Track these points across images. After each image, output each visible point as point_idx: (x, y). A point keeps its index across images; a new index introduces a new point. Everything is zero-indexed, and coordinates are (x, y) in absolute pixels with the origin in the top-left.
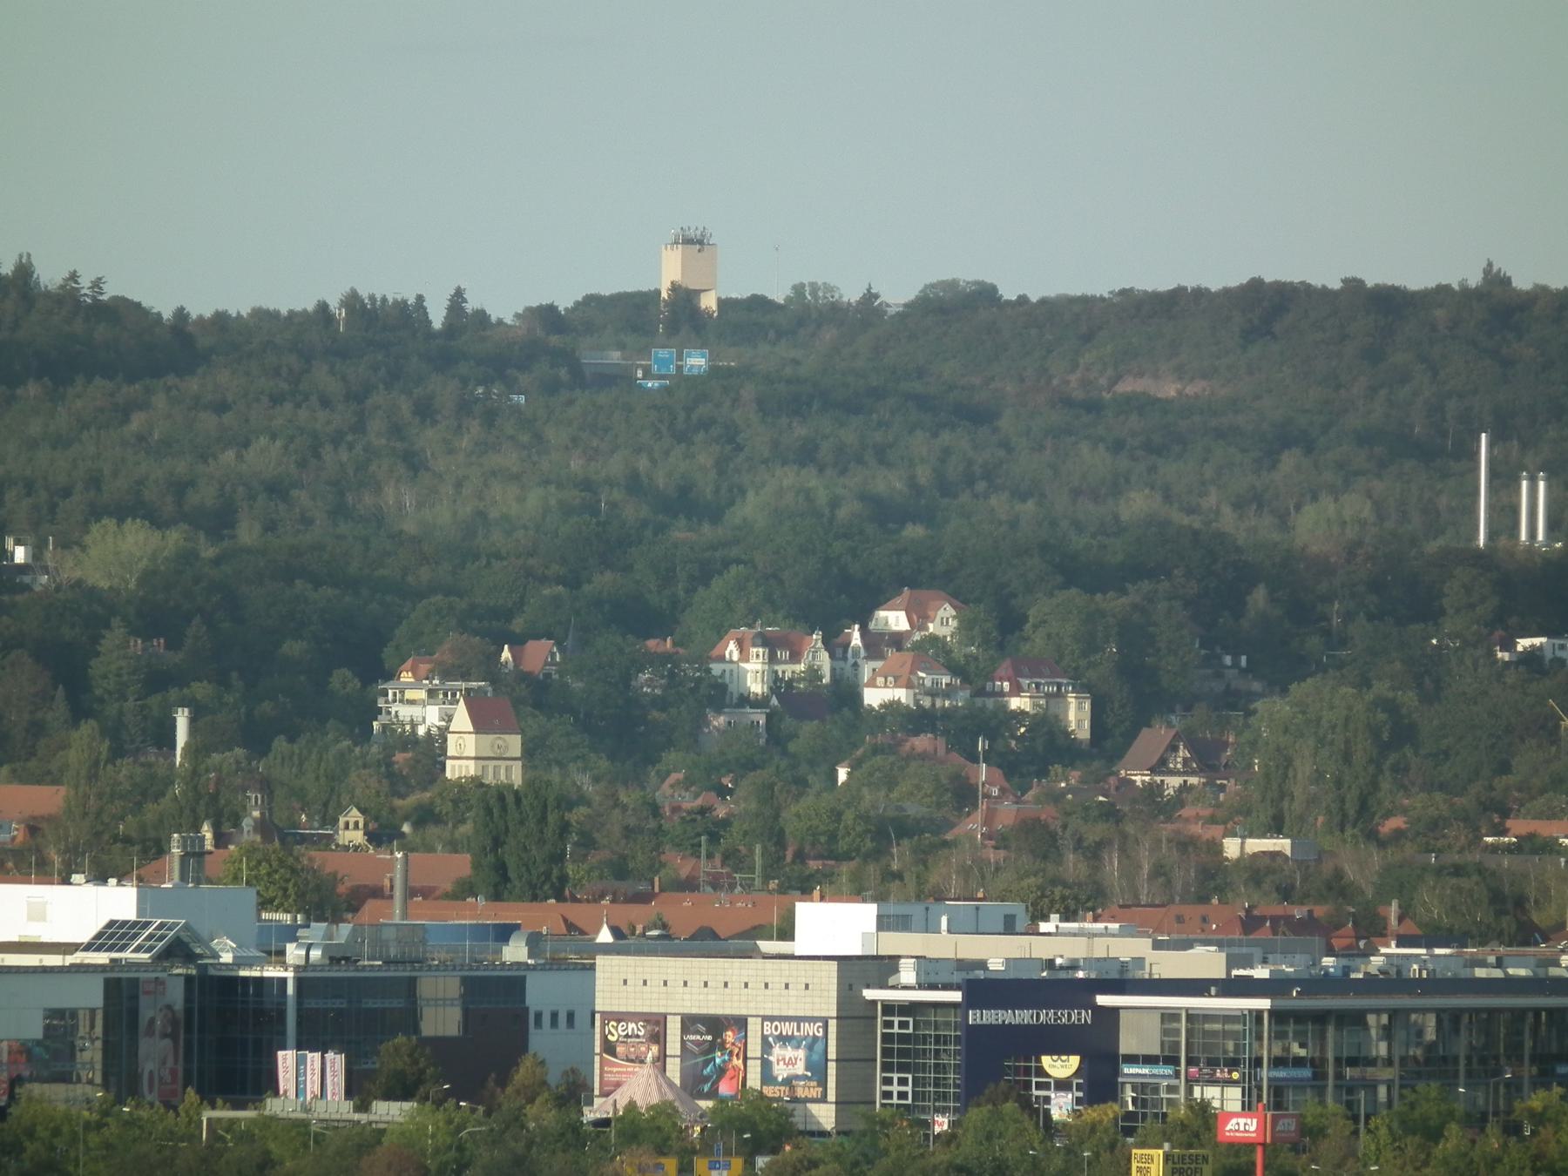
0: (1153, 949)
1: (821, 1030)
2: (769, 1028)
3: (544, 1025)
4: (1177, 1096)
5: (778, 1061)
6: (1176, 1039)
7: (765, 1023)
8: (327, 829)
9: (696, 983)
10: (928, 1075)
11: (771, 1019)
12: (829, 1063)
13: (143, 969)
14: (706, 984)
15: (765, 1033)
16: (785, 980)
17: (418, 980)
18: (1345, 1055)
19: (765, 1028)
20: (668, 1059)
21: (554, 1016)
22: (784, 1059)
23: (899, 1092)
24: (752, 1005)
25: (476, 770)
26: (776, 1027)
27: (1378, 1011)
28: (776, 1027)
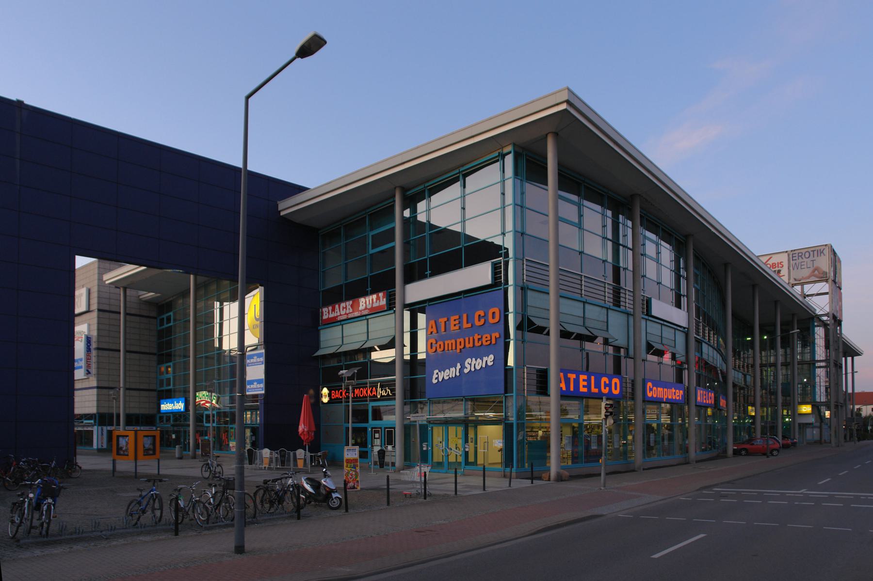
0: (326, 42)
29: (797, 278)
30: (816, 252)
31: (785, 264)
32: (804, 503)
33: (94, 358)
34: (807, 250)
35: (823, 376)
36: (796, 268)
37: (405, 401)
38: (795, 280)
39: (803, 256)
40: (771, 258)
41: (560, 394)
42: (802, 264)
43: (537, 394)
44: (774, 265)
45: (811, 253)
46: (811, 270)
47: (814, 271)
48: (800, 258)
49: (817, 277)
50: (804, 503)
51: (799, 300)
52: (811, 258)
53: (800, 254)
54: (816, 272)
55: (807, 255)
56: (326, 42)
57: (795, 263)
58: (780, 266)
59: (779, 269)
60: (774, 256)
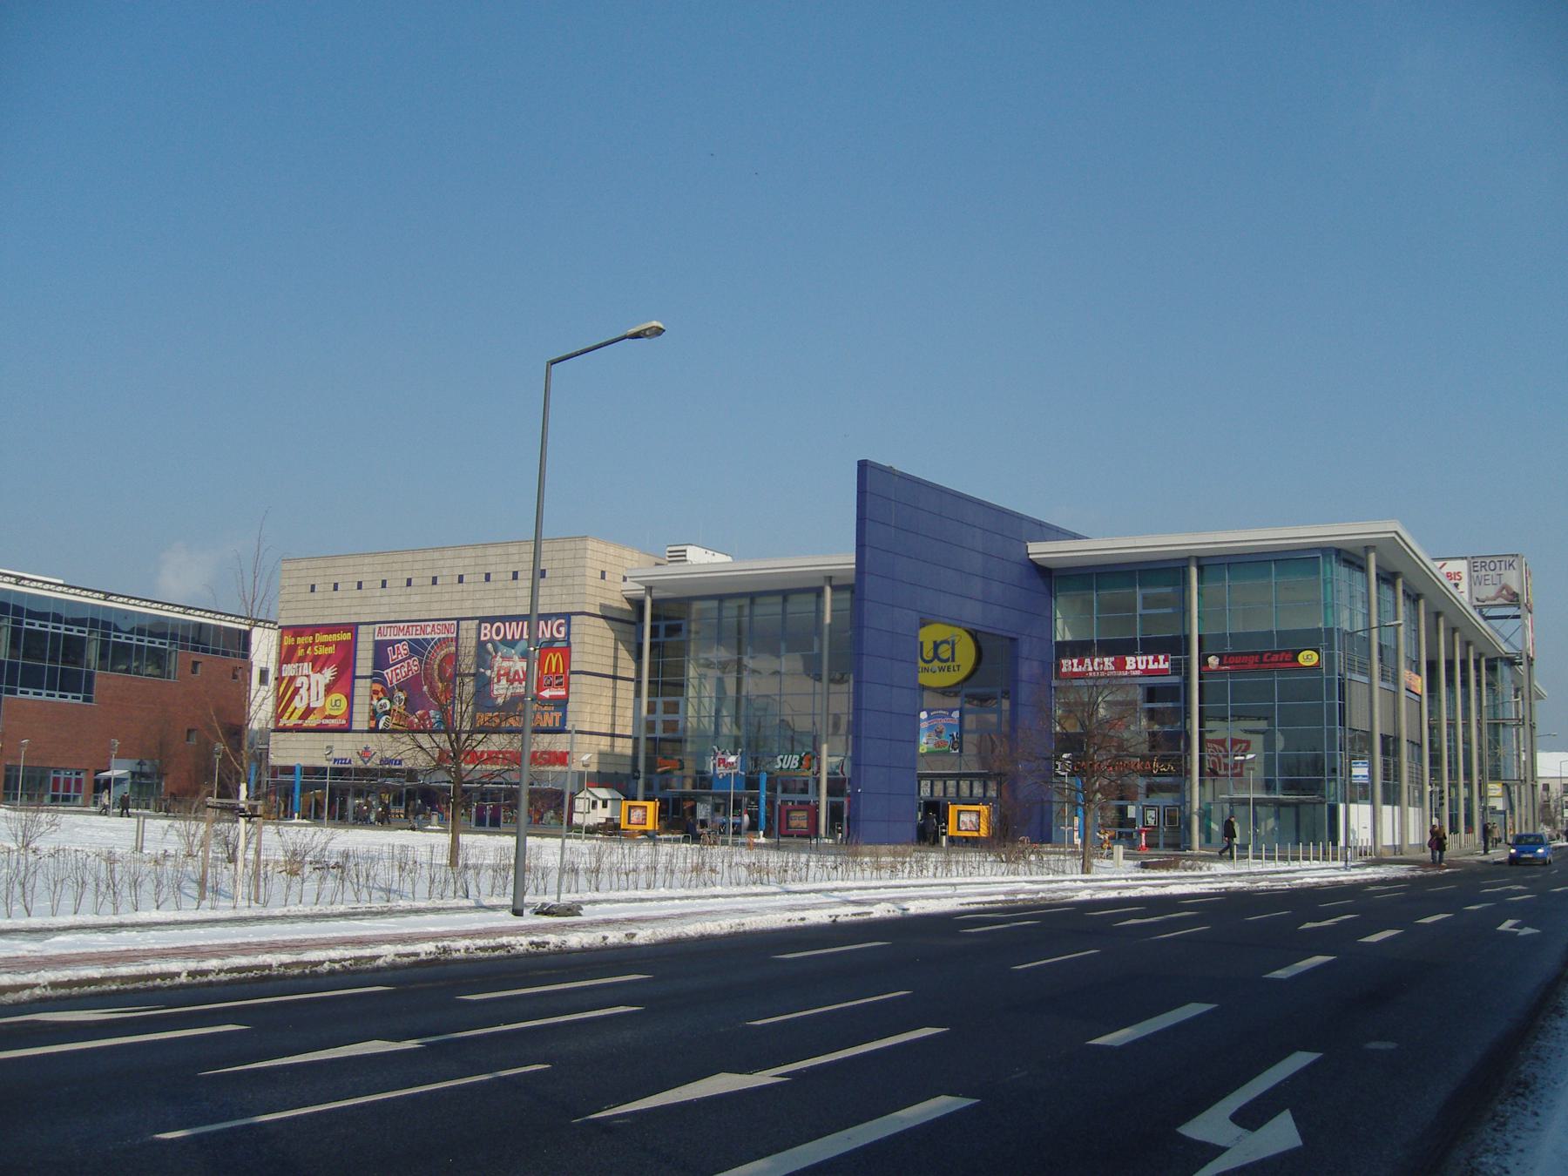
0: (858, 462)
1: (562, 629)
2: (487, 631)
3: (371, 646)
4: (1196, 844)
5: (499, 676)
6: (833, 799)
7: (483, 625)
8: (1488, 700)
9: (397, 581)
10: (328, 777)
11: (491, 620)
12: (358, 682)
13: (1452, 744)
14: (409, 583)
15: (483, 638)
16: (512, 568)
17: (1146, 699)
18: (586, 824)
19: (483, 632)
20: (357, 681)
21: (954, 670)
22: (507, 674)
23: (59, 778)
24: (468, 604)
25: (1364, 625)
26: (498, 629)
27: (620, 818)
28: (498, 629)
29: (1480, 598)
30: (1503, 563)
31: (1465, 575)
32: (759, 1023)
33: (649, 932)
34: (1492, 559)
35: (444, 903)
36: (1478, 584)
37: (351, 819)
38: (1478, 600)
39: (1487, 567)
40: (1444, 564)
41: (914, 855)
42: (1487, 578)
43: (938, 842)
44: (1449, 575)
45: (1498, 564)
46: (1499, 587)
47: (1502, 591)
48: (1483, 569)
49: (1507, 600)
50: (759, 1023)
51: (1486, 632)
52: (1498, 571)
53: (1483, 564)
54: (1504, 592)
55: (1492, 567)
56: (858, 462)
57: (1478, 577)
58: (1457, 577)
59: (1457, 581)
60: (1449, 562)
